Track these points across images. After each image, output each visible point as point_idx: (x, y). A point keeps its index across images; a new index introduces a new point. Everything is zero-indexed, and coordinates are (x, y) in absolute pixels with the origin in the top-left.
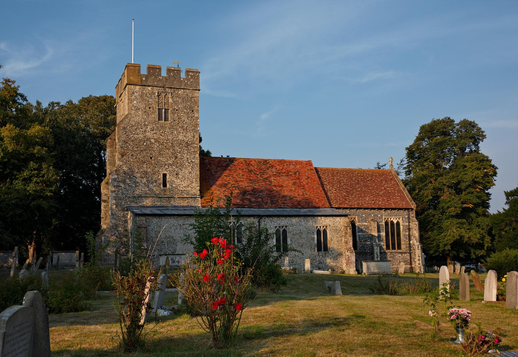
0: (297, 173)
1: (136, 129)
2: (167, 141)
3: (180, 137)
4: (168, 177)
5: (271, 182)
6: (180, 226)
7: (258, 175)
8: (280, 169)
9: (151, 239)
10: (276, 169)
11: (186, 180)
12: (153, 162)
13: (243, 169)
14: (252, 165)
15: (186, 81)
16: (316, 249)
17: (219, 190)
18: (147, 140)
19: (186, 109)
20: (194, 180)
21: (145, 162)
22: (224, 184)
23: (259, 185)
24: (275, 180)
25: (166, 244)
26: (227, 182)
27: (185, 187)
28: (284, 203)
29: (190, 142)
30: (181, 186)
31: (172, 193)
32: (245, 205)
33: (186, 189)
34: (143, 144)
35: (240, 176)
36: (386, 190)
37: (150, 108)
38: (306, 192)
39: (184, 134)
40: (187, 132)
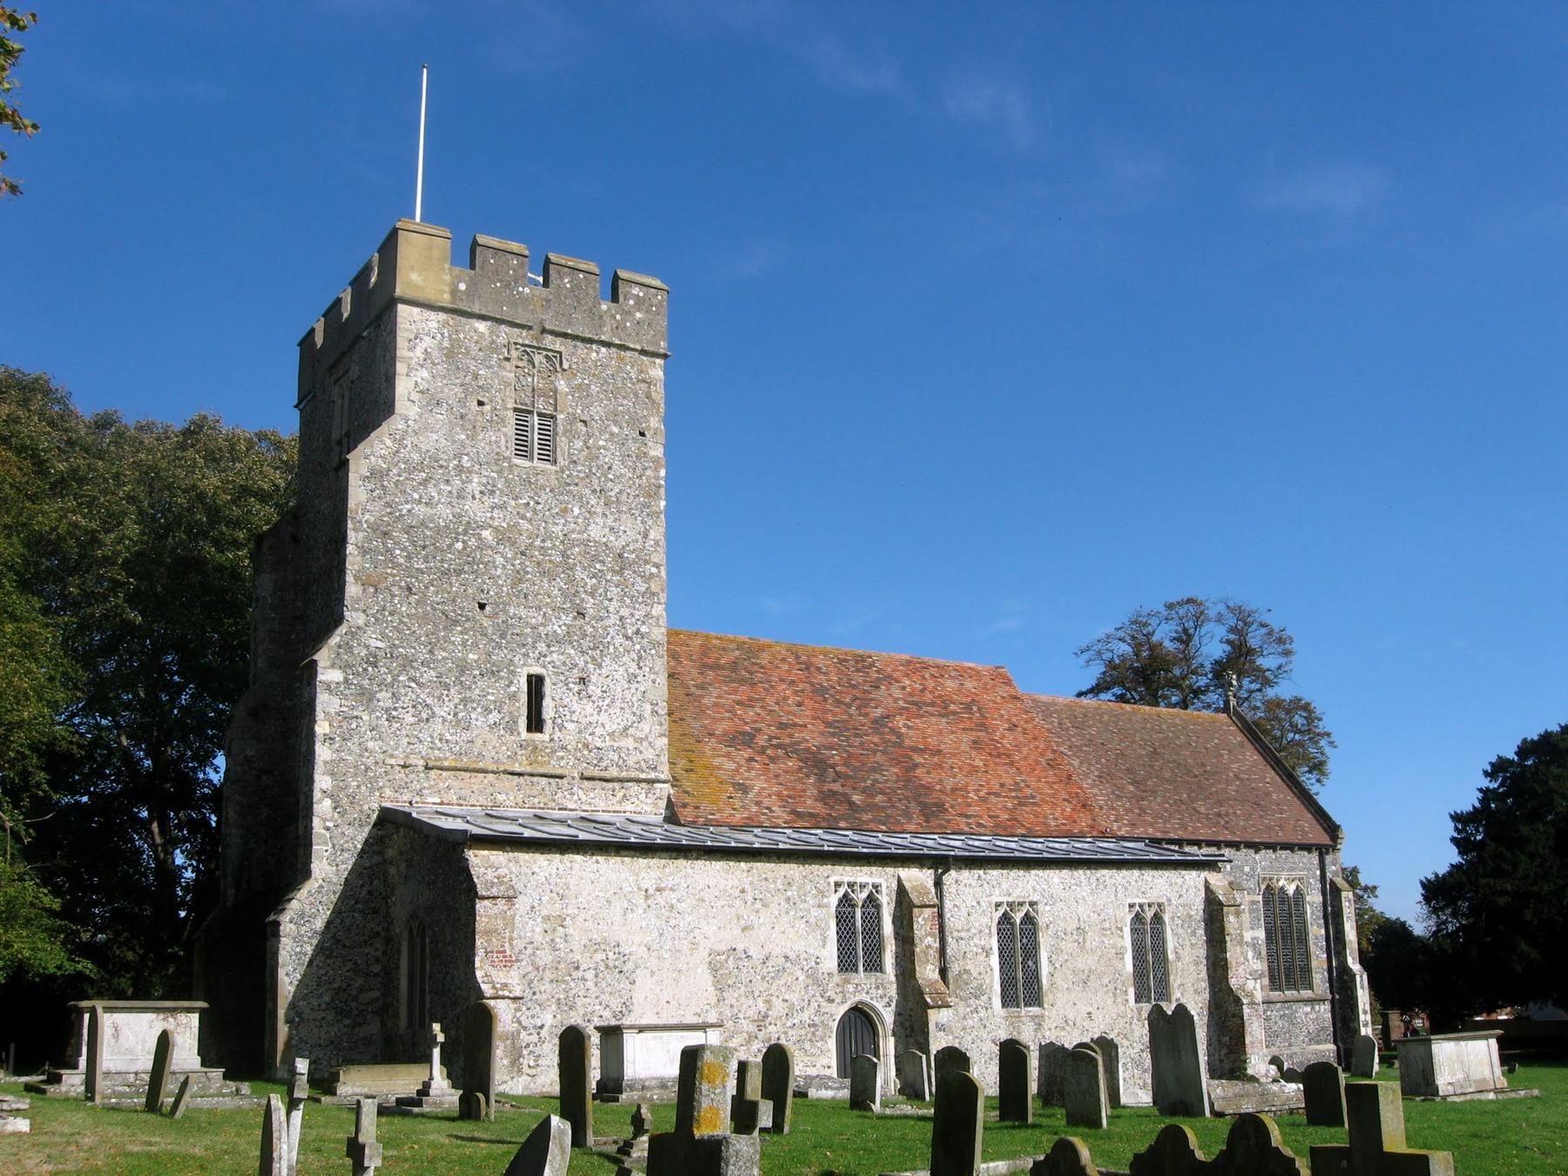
0: (975, 708)
1: (425, 483)
2: (543, 541)
3: (595, 532)
4: (548, 688)
5: (899, 735)
6: (647, 898)
7: (849, 706)
8: (913, 689)
9: (529, 951)
10: (904, 688)
11: (618, 704)
12: (486, 622)
13: (793, 682)
14: (818, 669)
15: (618, 317)
16: (1131, 991)
17: (728, 755)
18: (465, 532)
19: (616, 423)
20: (648, 707)
21: (456, 623)
22: (741, 733)
23: (862, 744)
24: (909, 728)
25: (590, 975)
26: (752, 728)
27: (611, 735)
28: (967, 816)
29: (633, 556)
30: (599, 731)
31: (562, 758)
32: (835, 818)
33: (616, 745)
34: (450, 546)
35: (789, 705)
36: (1241, 780)
37: (481, 403)
38: (1024, 777)
39: (610, 522)
40: (620, 512)
